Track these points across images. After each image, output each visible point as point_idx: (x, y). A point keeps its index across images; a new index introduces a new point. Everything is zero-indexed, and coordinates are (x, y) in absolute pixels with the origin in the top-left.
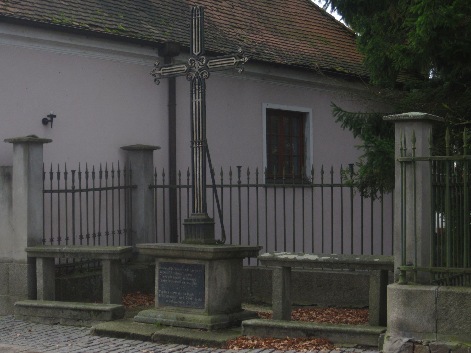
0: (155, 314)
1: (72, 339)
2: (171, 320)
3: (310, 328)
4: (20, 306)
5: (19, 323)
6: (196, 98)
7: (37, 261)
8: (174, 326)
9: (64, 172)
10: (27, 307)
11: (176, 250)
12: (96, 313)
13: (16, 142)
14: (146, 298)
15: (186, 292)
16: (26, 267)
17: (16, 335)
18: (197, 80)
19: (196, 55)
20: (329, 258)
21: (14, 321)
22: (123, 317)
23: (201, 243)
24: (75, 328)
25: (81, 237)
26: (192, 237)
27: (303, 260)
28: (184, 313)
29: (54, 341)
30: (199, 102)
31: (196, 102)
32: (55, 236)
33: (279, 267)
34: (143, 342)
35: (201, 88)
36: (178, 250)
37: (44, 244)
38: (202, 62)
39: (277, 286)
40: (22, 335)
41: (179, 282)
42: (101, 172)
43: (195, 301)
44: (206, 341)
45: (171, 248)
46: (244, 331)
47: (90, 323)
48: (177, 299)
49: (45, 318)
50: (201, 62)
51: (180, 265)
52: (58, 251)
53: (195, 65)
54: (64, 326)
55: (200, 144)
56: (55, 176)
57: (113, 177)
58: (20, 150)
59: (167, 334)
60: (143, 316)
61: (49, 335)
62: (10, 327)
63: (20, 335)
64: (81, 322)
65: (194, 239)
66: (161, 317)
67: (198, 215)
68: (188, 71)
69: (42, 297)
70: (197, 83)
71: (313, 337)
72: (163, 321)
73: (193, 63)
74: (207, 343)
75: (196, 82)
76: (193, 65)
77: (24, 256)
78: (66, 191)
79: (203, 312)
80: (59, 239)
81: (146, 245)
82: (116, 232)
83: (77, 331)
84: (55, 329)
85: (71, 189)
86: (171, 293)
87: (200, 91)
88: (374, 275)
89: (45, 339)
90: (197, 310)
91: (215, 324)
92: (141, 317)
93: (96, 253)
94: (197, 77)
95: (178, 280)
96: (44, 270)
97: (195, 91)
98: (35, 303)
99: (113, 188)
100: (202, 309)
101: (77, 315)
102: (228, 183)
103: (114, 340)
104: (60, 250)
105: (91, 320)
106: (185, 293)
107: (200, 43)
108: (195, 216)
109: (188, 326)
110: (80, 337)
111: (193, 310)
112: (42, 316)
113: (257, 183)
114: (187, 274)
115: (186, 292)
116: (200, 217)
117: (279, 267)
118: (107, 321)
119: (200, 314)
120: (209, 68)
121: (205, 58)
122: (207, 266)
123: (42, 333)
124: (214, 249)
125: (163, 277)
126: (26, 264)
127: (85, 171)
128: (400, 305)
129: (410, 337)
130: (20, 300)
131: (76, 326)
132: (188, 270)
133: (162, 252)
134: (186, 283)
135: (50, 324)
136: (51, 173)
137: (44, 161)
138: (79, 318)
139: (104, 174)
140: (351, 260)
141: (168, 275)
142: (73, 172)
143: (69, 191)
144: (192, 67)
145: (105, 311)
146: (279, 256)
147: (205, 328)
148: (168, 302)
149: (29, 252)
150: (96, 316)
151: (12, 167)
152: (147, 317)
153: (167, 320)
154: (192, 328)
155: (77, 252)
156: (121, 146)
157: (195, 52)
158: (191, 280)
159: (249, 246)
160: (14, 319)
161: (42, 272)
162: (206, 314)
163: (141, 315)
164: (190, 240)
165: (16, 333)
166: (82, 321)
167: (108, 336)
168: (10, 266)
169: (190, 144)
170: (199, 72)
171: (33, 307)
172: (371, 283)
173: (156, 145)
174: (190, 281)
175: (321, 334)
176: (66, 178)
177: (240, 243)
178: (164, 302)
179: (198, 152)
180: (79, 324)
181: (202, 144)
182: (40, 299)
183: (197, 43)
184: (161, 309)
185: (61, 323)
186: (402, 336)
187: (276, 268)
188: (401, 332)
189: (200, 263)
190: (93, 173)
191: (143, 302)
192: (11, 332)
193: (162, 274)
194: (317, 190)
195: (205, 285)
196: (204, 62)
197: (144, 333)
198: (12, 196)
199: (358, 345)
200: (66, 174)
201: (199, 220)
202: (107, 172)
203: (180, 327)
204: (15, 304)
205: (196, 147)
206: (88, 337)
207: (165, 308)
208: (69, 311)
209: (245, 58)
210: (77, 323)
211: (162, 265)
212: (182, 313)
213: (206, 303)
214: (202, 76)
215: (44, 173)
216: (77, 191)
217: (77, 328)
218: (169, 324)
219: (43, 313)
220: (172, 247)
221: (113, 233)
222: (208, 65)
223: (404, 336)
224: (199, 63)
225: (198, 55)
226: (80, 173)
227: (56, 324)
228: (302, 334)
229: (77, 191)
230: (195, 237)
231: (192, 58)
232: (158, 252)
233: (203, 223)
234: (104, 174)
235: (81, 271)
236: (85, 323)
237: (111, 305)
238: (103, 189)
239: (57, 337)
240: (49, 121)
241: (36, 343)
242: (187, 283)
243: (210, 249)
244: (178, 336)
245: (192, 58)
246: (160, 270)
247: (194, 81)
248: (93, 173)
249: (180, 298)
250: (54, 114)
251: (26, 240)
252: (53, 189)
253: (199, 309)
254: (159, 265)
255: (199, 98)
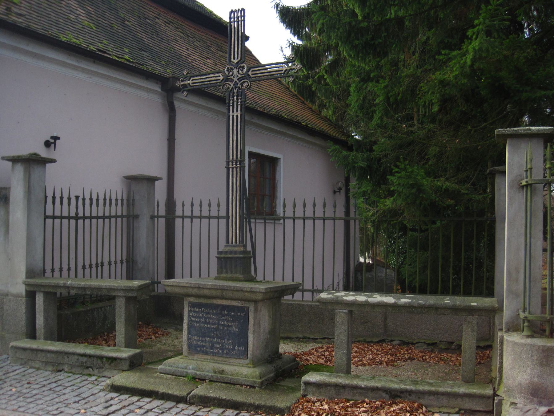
0: (186, 365)
1: (84, 399)
2: (207, 374)
3: (396, 388)
4: (17, 348)
5: (15, 368)
6: (233, 111)
7: (37, 296)
8: (210, 381)
9: (68, 197)
10: (24, 349)
11: (214, 289)
12: (110, 361)
13: (15, 160)
14: (150, 330)
15: (224, 339)
16: (24, 301)
17: (11, 390)
18: (235, 91)
19: (235, 62)
20: (410, 301)
21: (9, 365)
22: (141, 364)
23: (240, 281)
24: (83, 379)
25: (84, 267)
26: (227, 272)
27: (377, 303)
28: (222, 364)
29: (60, 402)
30: (237, 116)
31: (233, 116)
32: (57, 266)
33: (344, 311)
34: (177, 404)
35: (241, 99)
36: (217, 289)
37: (44, 275)
38: (242, 70)
39: (341, 333)
40: (19, 389)
41: (215, 326)
42: (105, 200)
43: (235, 350)
44: (263, 406)
45: (208, 287)
46: (305, 390)
47: (103, 372)
48: (212, 347)
49: (47, 363)
50: (241, 70)
51: (216, 307)
52: (62, 285)
53: (233, 74)
54: (70, 374)
55: (238, 163)
56: (58, 200)
57: (117, 205)
58: (20, 169)
59: (208, 395)
60: (169, 366)
61: (53, 390)
62: (4, 374)
63: (16, 391)
64: (91, 370)
65: (229, 275)
66: (194, 369)
67: (234, 246)
68: (224, 81)
69: (42, 337)
70: (235, 94)
71: (398, 400)
72: (196, 373)
73: (231, 71)
74: (264, 409)
75: (234, 93)
76: (231, 73)
77: (21, 289)
78: (69, 218)
79: (247, 363)
80: (61, 269)
81: (175, 282)
82: (119, 262)
83: (87, 382)
84: (60, 380)
85: (75, 215)
86: (204, 339)
87: (239, 103)
88: (468, 322)
89: (48, 398)
90: (237, 361)
91: (263, 379)
92: (167, 367)
93: (108, 289)
94: (236, 88)
95: (213, 324)
96: (44, 306)
97: (233, 103)
98: (34, 345)
99: (116, 217)
100: (245, 359)
101: (86, 362)
102: (189, 214)
103: (138, 401)
104: (64, 284)
105: (103, 368)
106: (222, 340)
107: (240, 49)
108: (230, 248)
109: (229, 382)
110: (93, 395)
111: (233, 360)
112: (43, 360)
113: (219, 214)
114: (224, 318)
115: (224, 339)
116: (236, 249)
117: (344, 311)
118: (123, 371)
119: (242, 366)
120: (250, 77)
121: (245, 66)
122: (252, 308)
123: (44, 386)
124: (266, 289)
125: (194, 319)
126: (24, 299)
127: (89, 197)
128: (534, 365)
129: (548, 406)
130: (16, 340)
131: (84, 375)
132: (226, 313)
133: (195, 291)
134: (223, 328)
135: (53, 371)
136: (54, 198)
137: (46, 184)
138: (88, 366)
139: (108, 202)
140: (441, 304)
141: (200, 318)
142: (77, 197)
143: (72, 218)
144: (229, 76)
145: (121, 359)
146: (344, 298)
147: (252, 384)
148: (201, 349)
149: (27, 285)
150: (110, 364)
151: (10, 188)
152: (176, 369)
153: (202, 373)
154: (235, 384)
155: (85, 286)
156: (124, 175)
157: (234, 59)
158: (230, 324)
159: (293, 283)
160: (9, 362)
161: (42, 307)
162: (249, 365)
163: (168, 365)
164: (224, 275)
165: (11, 386)
166: (92, 369)
167: (129, 394)
168: (5, 300)
169: (225, 163)
170: (238, 82)
171: (32, 350)
172: (465, 331)
173: (159, 176)
174: (228, 326)
175: (410, 395)
176: (69, 204)
177: (293, 281)
178: (194, 349)
179: (234, 173)
180: (88, 372)
181: (240, 164)
182: (39, 339)
183: (236, 50)
184: (191, 357)
185: (66, 369)
186: (537, 405)
187: (340, 312)
188: (535, 399)
189: (242, 304)
190: (98, 200)
191: (149, 335)
192: (5, 385)
193: (193, 317)
194: (289, 223)
195: (249, 331)
196: (245, 70)
197: (178, 392)
198: (8, 222)
199: (460, 410)
200: (69, 199)
201: (236, 253)
202: (111, 200)
203: (219, 382)
204: (10, 346)
205: (233, 168)
206: (102, 394)
207: (196, 357)
208: (76, 357)
209: (297, 65)
210: (86, 371)
211: (193, 305)
212: (219, 363)
213: (250, 353)
214: (242, 86)
215: (46, 197)
216: (80, 218)
217: (86, 377)
218: (204, 378)
219: (44, 357)
220: (208, 285)
221: (116, 263)
222: (250, 73)
223: (540, 404)
224: (238, 71)
225: (238, 63)
226: (84, 200)
227: (60, 371)
228: (384, 395)
229: (80, 218)
230: (232, 273)
231: (230, 66)
232: (190, 291)
233: (241, 256)
234: (108, 202)
235: (83, 303)
236: (96, 371)
237: (126, 349)
238: (107, 217)
239: (64, 394)
240: (52, 143)
241: (39, 407)
242: (226, 328)
243: (260, 289)
244: (224, 398)
245: (230, 66)
246: (189, 311)
247: (232, 91)
248: (98, 200)
249: (215, 345)
250: (58, 136)
251: (25, 272)
252: (63, 215)
253: (241, 359)
254: (189, 306)
255: (237, 111)
